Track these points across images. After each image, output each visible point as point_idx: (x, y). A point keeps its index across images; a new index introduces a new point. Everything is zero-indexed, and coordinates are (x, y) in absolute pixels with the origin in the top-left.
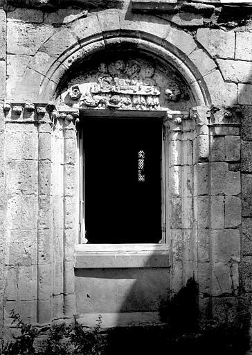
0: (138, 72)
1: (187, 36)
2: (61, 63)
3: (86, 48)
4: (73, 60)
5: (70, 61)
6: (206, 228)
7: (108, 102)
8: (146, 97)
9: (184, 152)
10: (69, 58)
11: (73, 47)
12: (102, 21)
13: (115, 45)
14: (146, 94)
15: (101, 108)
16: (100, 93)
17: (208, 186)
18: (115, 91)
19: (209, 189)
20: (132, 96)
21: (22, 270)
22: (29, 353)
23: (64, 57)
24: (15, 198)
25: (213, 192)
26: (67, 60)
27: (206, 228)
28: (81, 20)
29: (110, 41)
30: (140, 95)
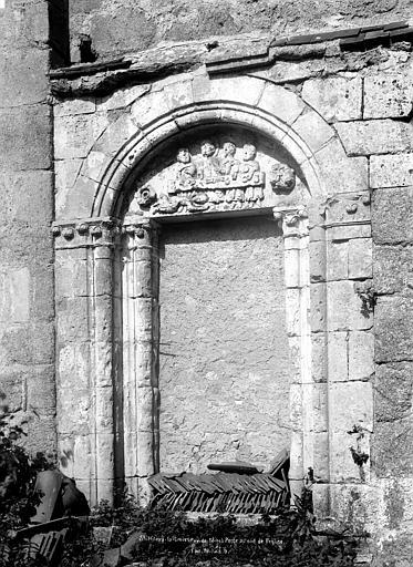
0: (233, 154)
1: (289, 96)
2: (121, 161)
3: (150, 137)
4: (136, 155)
5: (131, 158)
6: (321, 381)
7: (189, 204)
8: (244, 189)
9: (139, 304)
10: (129, 155)
11: (134, 137)
12: (170, 96)
13: (190, 126)
14: (244, 185)
15: (184, 213)
16: (177, 192)
17: (324, 318)
18: (200, 186)
19: (325, 321)
20: (224, 190)
21: (78, 440)
22: (342, 564)
23: (123, 153)
24: (68, 347)
25: (332, 326)
26: (127, 157)
27: (321, 381)
28: (144, 98)
29: (182, 121)
30: (236, 188)
